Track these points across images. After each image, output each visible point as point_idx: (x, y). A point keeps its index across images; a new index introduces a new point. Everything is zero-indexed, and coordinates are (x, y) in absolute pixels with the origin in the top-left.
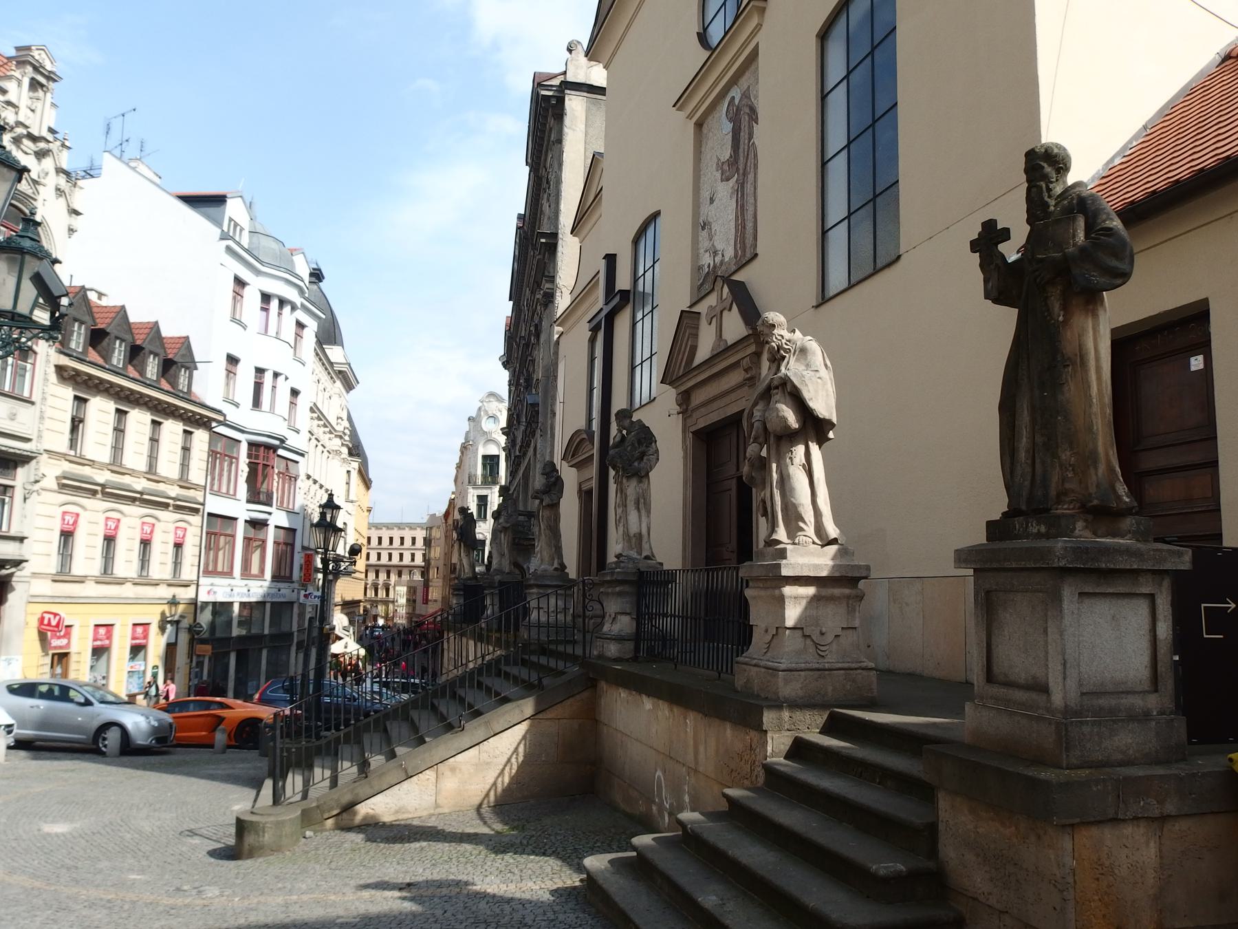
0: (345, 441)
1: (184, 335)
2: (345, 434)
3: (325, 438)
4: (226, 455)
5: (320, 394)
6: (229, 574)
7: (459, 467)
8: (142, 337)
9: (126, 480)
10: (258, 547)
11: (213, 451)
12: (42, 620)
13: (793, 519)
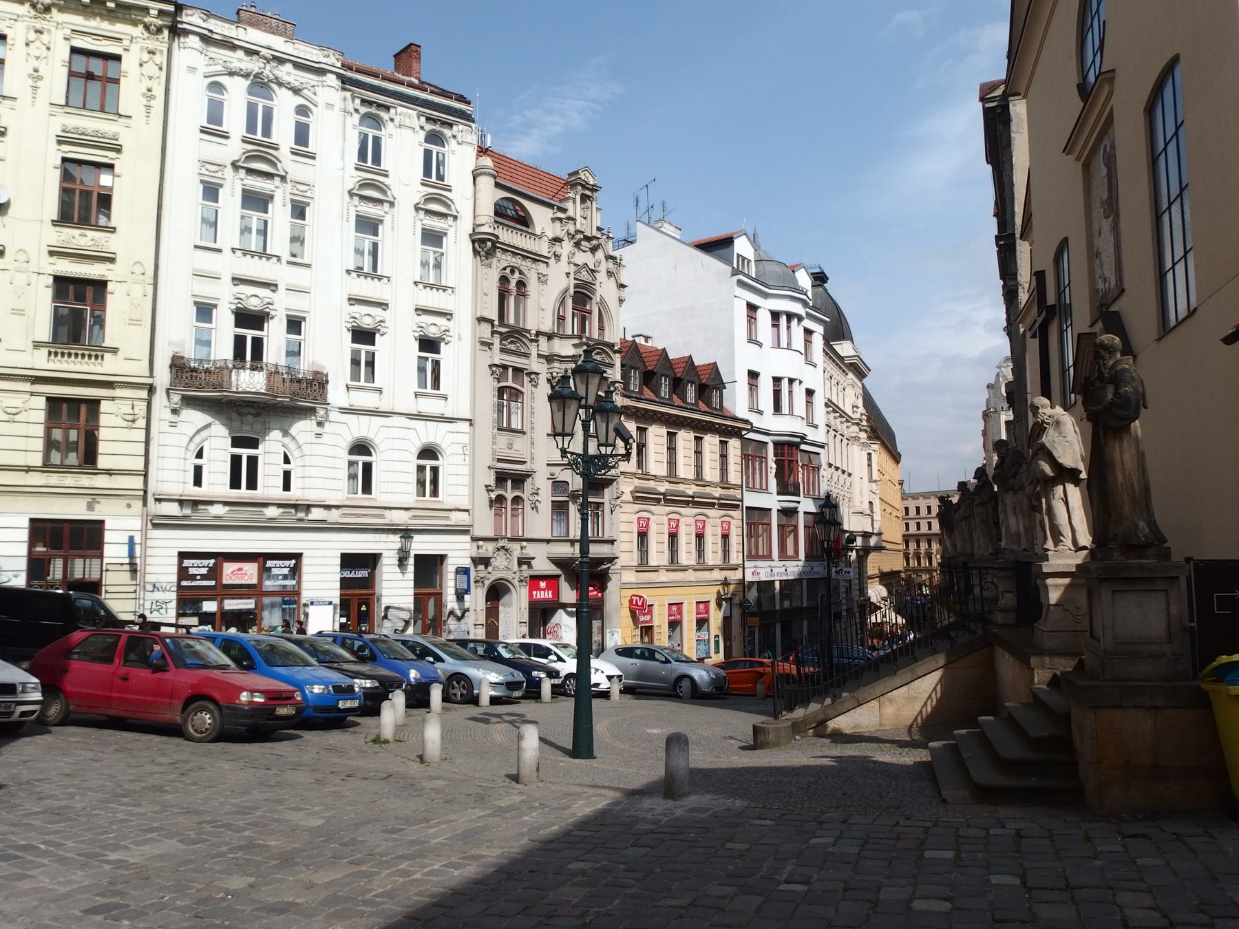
0: (863, 426)
1: (712, 361)
2: (861, 420)
3: (842, 428)
4: (756, 457)
5: (834, 389)
6: (768, 557)
7: (985, 433)
8: (681, 370)
9: (681, 487)
10: (791, 531)
11: (745, 454)
12: (631, 601)
13: (1057, 535)
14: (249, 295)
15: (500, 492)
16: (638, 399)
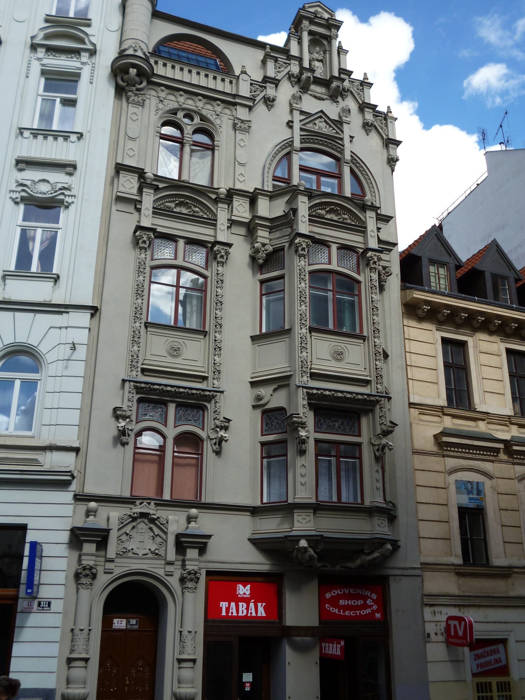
12: (448, 626)
14: (37, 181)
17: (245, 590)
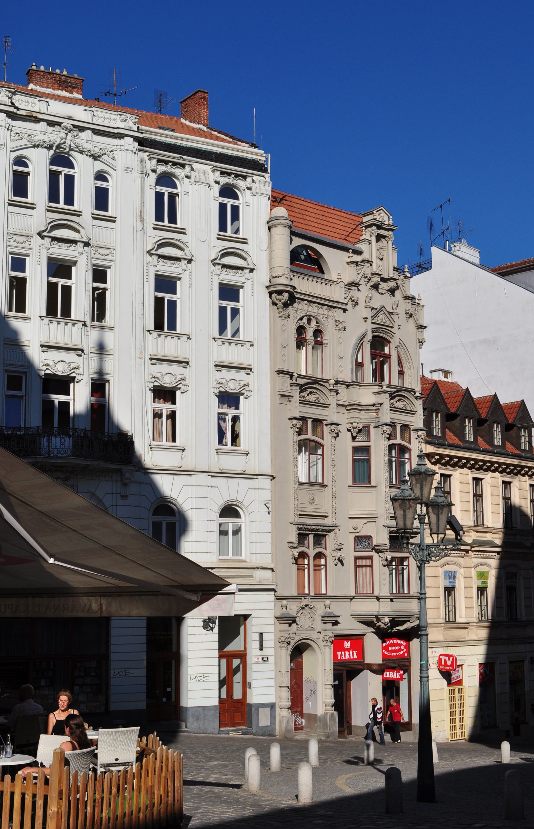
12: (440, 660)
15: (302, 549)
16: (441, 445)
17: (348, 644)
